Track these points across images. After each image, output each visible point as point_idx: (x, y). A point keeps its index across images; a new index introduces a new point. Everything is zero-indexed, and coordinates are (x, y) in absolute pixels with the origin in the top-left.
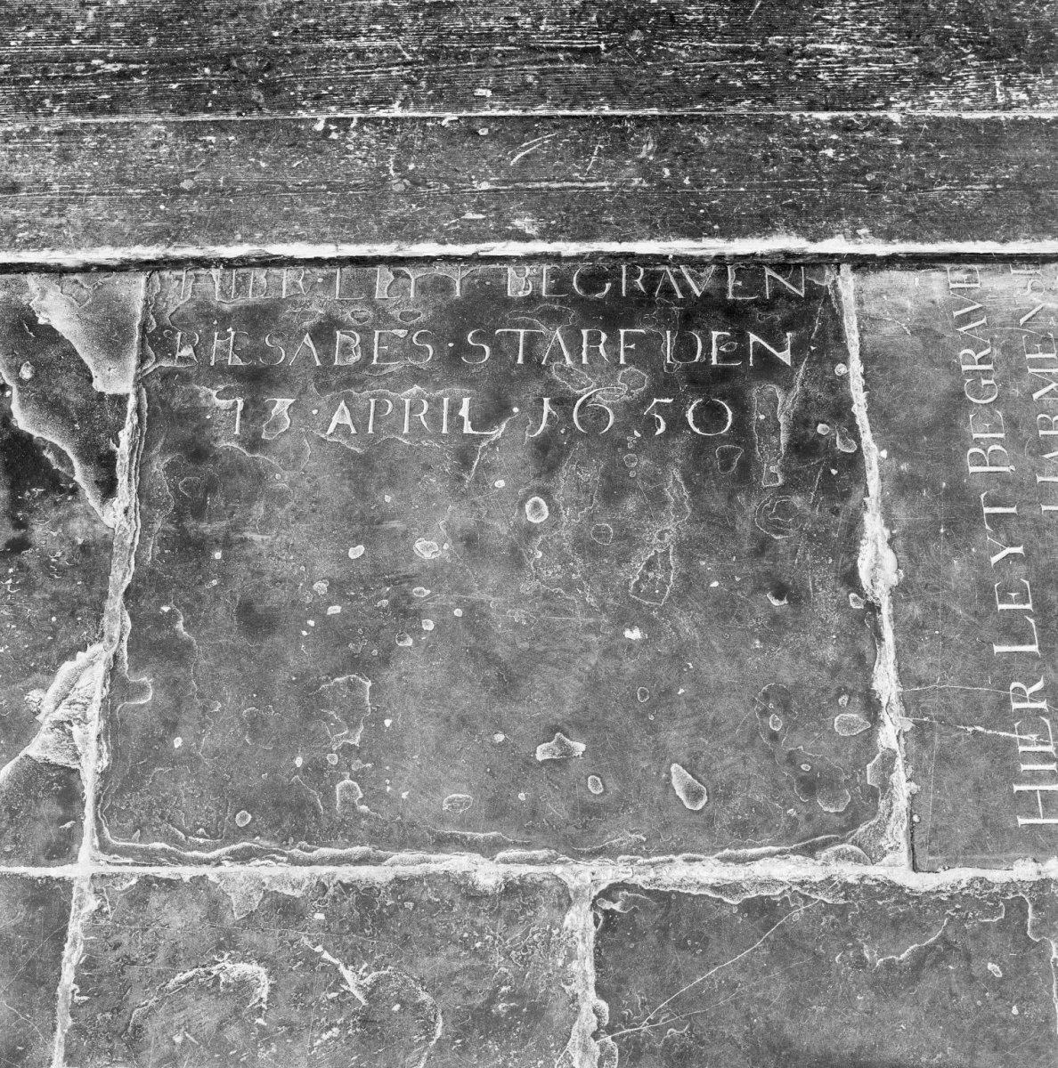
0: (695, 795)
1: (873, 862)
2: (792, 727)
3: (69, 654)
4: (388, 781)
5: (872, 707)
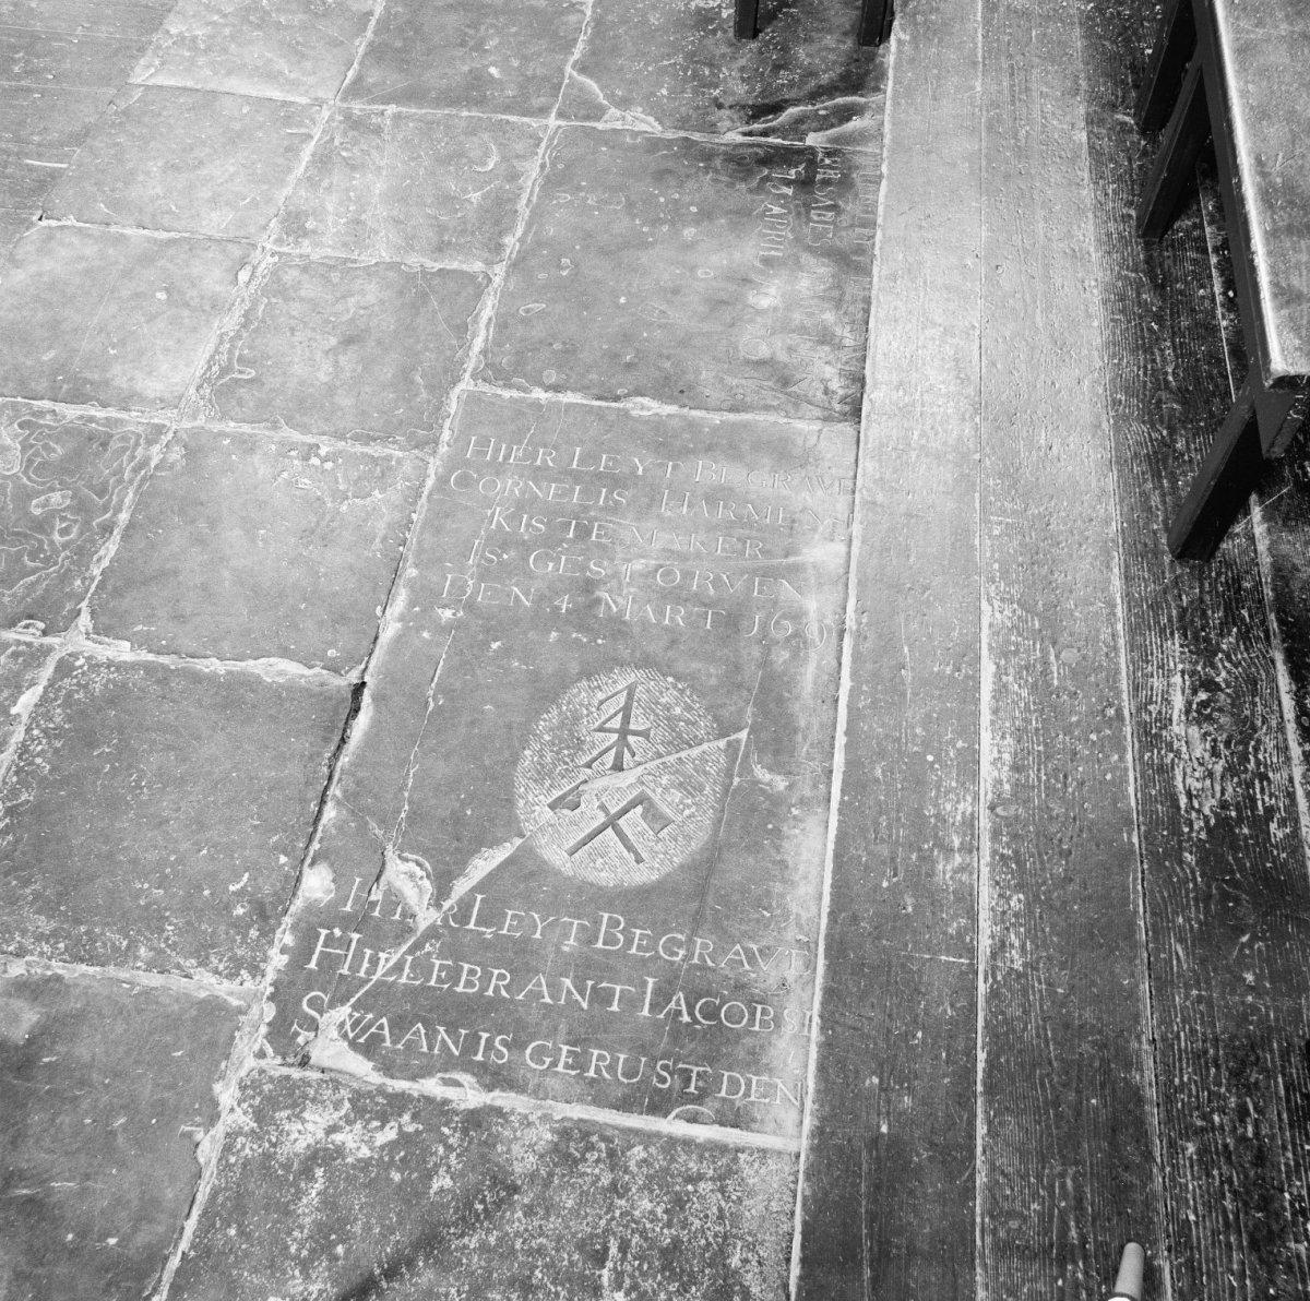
0: (527, 311)
1: (472, 376)
2: (554, 352)
3: (657, 119)
4: (868, 1082)
5: (557, 388)
